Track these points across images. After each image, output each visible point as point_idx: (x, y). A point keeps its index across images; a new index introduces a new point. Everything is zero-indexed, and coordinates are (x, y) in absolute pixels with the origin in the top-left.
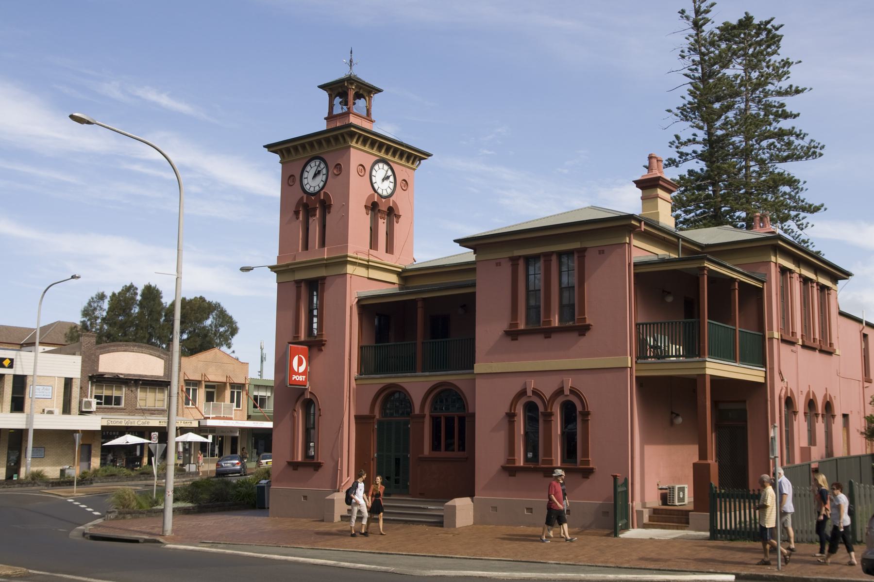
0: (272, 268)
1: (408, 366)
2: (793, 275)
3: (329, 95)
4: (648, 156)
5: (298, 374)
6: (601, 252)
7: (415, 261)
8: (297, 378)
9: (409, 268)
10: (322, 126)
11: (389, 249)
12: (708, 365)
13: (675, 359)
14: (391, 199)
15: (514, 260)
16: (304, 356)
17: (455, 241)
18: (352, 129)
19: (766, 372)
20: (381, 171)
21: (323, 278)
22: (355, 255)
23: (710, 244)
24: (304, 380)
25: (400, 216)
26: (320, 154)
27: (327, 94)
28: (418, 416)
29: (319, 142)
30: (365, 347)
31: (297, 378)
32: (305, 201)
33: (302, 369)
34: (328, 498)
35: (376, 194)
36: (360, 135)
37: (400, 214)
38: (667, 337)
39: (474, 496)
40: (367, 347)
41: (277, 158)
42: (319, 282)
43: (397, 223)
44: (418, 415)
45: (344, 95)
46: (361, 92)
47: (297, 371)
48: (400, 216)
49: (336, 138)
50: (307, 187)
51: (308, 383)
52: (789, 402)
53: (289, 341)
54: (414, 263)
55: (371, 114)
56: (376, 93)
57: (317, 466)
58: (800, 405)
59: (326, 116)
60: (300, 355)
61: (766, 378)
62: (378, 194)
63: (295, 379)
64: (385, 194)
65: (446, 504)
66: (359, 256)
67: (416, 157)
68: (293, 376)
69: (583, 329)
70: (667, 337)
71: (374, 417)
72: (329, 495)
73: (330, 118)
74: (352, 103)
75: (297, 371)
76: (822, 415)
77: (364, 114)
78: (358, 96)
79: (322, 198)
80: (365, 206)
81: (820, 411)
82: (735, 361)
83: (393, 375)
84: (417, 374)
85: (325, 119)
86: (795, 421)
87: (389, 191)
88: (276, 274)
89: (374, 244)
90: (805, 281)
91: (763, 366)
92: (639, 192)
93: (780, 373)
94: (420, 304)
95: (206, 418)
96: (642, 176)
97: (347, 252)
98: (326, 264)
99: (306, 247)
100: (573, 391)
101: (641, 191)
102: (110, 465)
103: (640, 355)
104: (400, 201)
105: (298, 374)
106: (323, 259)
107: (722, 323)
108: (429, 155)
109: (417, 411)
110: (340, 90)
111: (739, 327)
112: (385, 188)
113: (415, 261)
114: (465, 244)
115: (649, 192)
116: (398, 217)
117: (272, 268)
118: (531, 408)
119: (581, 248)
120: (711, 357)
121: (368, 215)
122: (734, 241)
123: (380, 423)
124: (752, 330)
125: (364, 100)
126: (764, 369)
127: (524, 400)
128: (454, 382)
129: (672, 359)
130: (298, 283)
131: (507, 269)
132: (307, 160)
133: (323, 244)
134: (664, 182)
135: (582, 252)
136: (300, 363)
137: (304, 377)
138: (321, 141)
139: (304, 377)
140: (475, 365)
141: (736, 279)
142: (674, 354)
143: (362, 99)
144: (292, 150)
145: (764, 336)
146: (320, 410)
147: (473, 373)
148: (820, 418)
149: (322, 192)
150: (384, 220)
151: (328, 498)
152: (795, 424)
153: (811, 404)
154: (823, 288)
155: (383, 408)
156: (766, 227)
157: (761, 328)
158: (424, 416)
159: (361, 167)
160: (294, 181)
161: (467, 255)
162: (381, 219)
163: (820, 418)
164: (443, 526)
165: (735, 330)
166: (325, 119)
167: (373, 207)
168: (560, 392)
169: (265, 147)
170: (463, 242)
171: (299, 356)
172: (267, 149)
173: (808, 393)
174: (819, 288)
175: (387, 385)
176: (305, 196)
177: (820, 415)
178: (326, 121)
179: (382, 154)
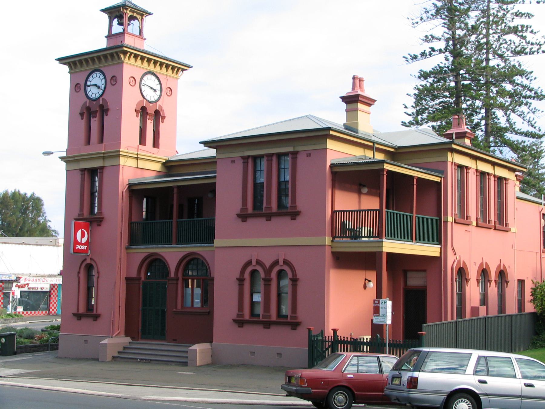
0: (62, 158)
1: (167, 240)
2: (470, 171)
3: (109, 17)
4: (352, 77)
5: (81, 244)
6: (309, 155)
7: (178, 153)
8: (81, 247)
9: (172, 159)
10: (102, 44)
11: (156, 144)
12: (384, 244)
13: (367, 239)
14: (158, 103)
15: (245, 159)
16: (85, 230)
17: (200, 143)
18: (125, 49)
19: (441, 248)
20: (150, 80)
21: (102, 168)
22: (127, 151)
23: (402, 147)
24: (86, 249)
25: (165, 117)
26: (101, 67)
27: (107, 16)
28: (172, 279)
29: (99, 58)
30: (134, 223)
31: (81, 247)
32: (88, 105)
33: (84, 240)
34: (103, 342)
35: (145, 100)
36: (131, 53)
37: (165, 116)
38: (347, 227)
39: (213, 342)
40: (139, 223)
41: (66, 68)
42: (99, 171)
43: (162, 123)
44: (173, 278)
45: (120, 17)
46: (135, 15)
47: (80, 242)
48: (165, 117)
49: (112, 55)
50: (90, 94)
51: (89, 251)
52: (462, 272)
53: (75, 218)
54: (177, 155)
55: (142, 33)
56: (147, 16)
57: (96, 317)
58: (473, 273)
59: (107, 34)
60: (83, 230)
61: (441, 253)
62: (147, 100)
63: (78, 248)
64: (152, 100)
65: (190, 348)
66: (129, 151)
67: (179, 68)
68: (77, 246)
69: (294, 214)
70: (347, 227)
71: (140, 278)
72: (103, 340)
73: (110, 36)
74: (127, 24)
75: (80, 242)
76: (495, 281)
77: (138, 33)
78: (132, 18)
79: (101, 103)
80: (135, 110)
81: (493, 278)
82: (412, 241)
83: (155, 246)
84: (172, 245)
85: (106, 37)
86: (467, 286)
87: (156, 98)
88: (65, 163)
89: (142, 141)
90: (483, 175)
91: (438, 243)
92: (344, 105)
93: (453, 249)
94: (175, 190)
95: (417, 127)
96: (347, 93)
97: (120, 148)
98: (104, 157)
99: (88, 142)
100: (286, 262)
101: (346, 105)
102: (436, 126)
103: (341, 235)
104: (165, 105)
105: (81, 244)
106: (101, 153)
107: (406, 212)
108: (190, 67)
109: (172, 275)
110: (118, 14)
111: (416, 214)
112: (151, 96)
113: (178, 153)
114: (209, 145)
115: (352, 106)
116: (164, 118)
117: (62, 158)
118: (254, 273)
119: (294, 151)
120: (388, 238)
121: (137, 117)
122: (420, 145)
123: (145, 284)
124: (432, 216)
125: (137, 21)
126: (440, 246)
127: (249, 269)
128: (200, 253)
129: (363, 239)
130: (83, 170)
131: (239, 166)
132: (90, 71)
133: (101, 140)
134: (363, 98)
135: (295, 154)
136: (83, 236)
137: (86, 246)
138: (94, 58)
139: (86, 246)
140: (214, 240)
141: (414, 176)
142: (366, 236)
143: (136, 20)
144: (83, 62)
145: (440, 220)
146: (98, 272)
147: (213, 246)
148: (493, 283)
149: (101, 98)
150: (151, 120)
151: (103, 342)
152: (467, 289)
153: (484, 273)
154: (500, 180)
155: (148, 270)
156: (461, 128)
157: (439, 215)
158: (177, 279)
159: (132, 79)
160: (80, 88)
161: (212, 152)
162: (149, 120)
163: (493, 283)
164: (187, 366)
165: (413, 217)
166: (106, 37)
167: (143, 112)
168: (276, 263)
169: (56, 60)
170: (207, 144)
171: (81, 230)
172: (58, 62)
173: (482, 264)
174: (496, 179)
175: (150, 254)
176: (88, 101)
177: (493, 282)
178: (106, 38)
179: (151, 67)
